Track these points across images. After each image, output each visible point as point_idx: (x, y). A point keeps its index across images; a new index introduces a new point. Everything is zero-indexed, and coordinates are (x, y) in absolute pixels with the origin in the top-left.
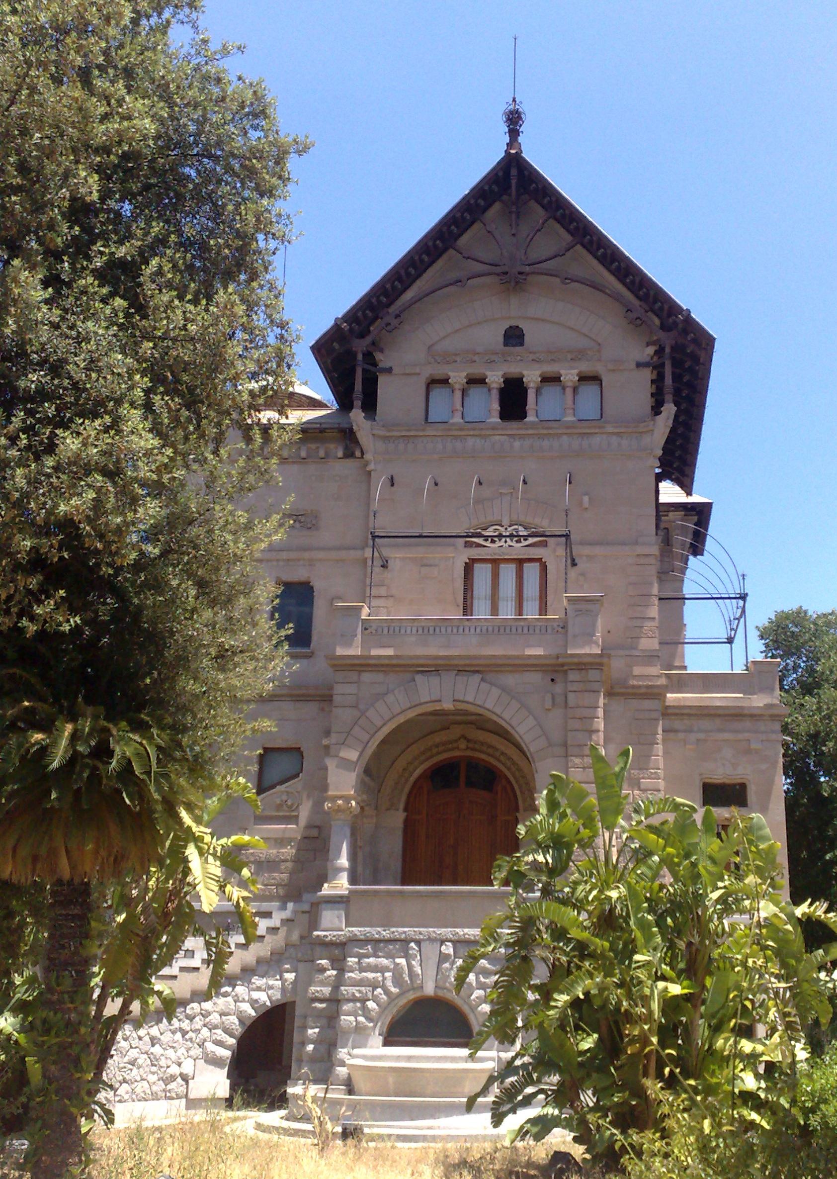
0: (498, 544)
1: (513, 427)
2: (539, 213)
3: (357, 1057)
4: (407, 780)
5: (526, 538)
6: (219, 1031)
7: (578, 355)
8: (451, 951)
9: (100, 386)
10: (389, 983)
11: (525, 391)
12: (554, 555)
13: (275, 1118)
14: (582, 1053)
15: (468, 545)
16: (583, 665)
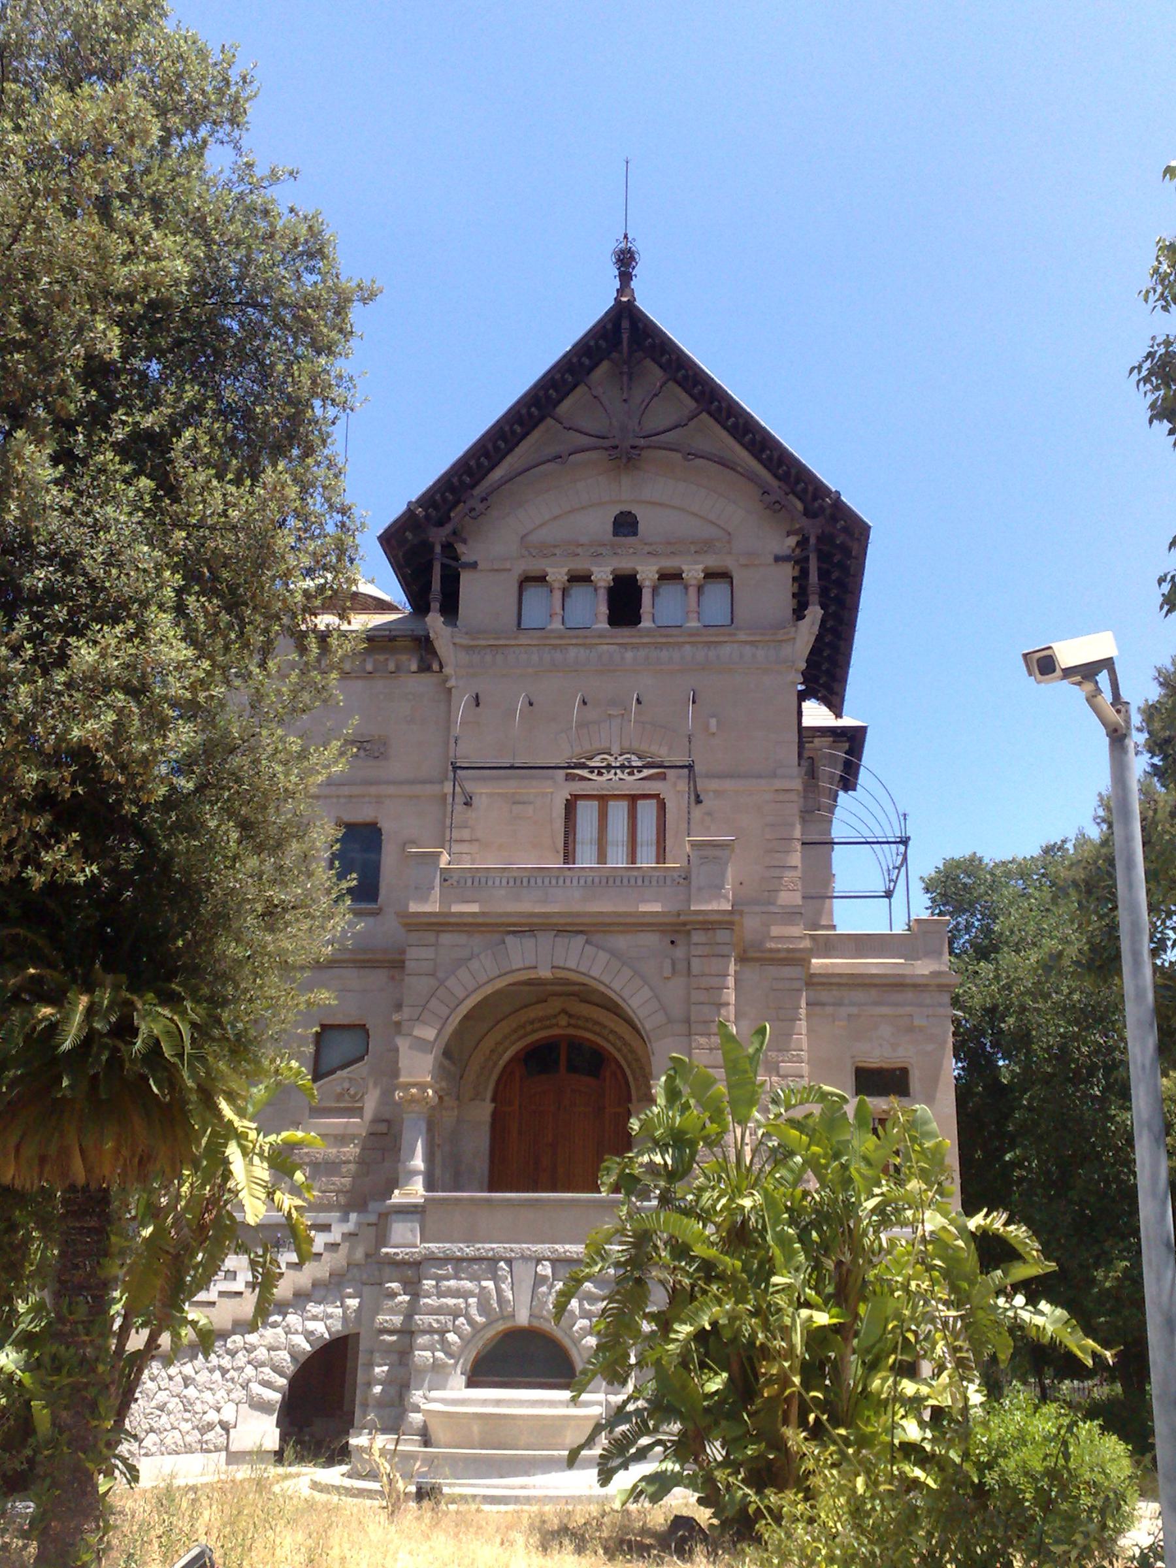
0: (606, 777)
1: (624, 634)
2: (656, 374)
4: (495, 1064)
5: (639, 769)
6: (267, 1370)
7: (705, 546)
8: (549, 1272)
10: (473, 1311)
11: (639, 590)
12: (673, 790)
13: (334, 1475)
15: (569, 778)
16: (709, 924)
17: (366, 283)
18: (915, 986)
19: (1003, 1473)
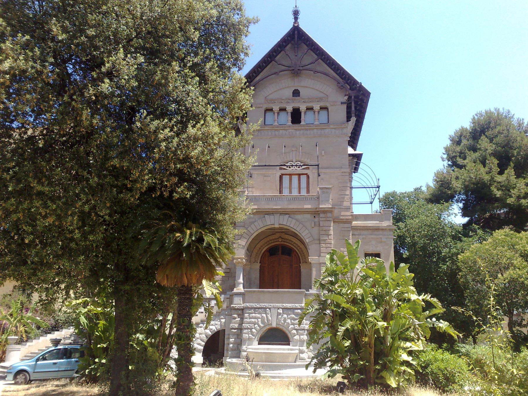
0: (292, 168)
1: (296, 126)
2: (305, 47)
3: (250, 349)
4: (261, 252)
5: (301, 166)
6: (199, 340)
7: (320, 100)
8: (281, 312)
9: (196, 109)
10: (260, 323)
11: (300, 113)
12: (312, 172)
13: (222, 370)
14: (346, 347)
15: (281, 169)
16: (325, 211)
17: (255, 18)
18: (382, 229)
19: (432, 369)
